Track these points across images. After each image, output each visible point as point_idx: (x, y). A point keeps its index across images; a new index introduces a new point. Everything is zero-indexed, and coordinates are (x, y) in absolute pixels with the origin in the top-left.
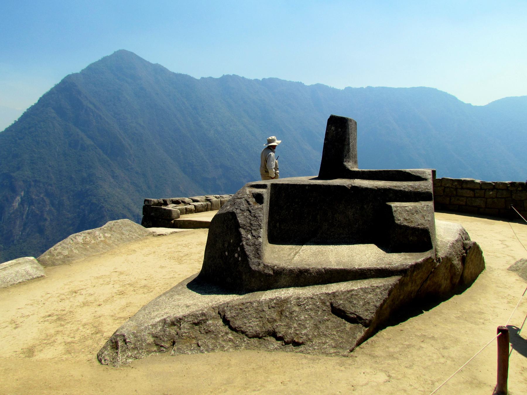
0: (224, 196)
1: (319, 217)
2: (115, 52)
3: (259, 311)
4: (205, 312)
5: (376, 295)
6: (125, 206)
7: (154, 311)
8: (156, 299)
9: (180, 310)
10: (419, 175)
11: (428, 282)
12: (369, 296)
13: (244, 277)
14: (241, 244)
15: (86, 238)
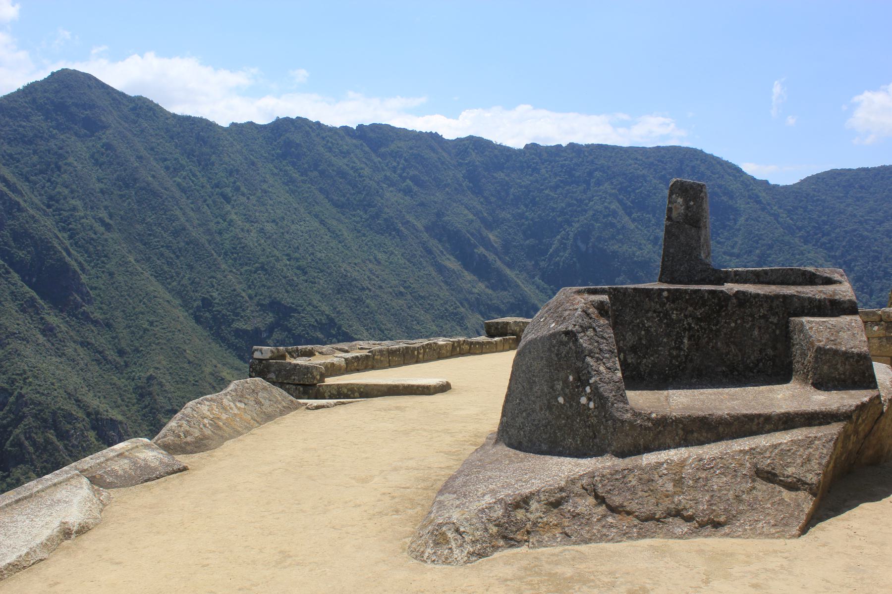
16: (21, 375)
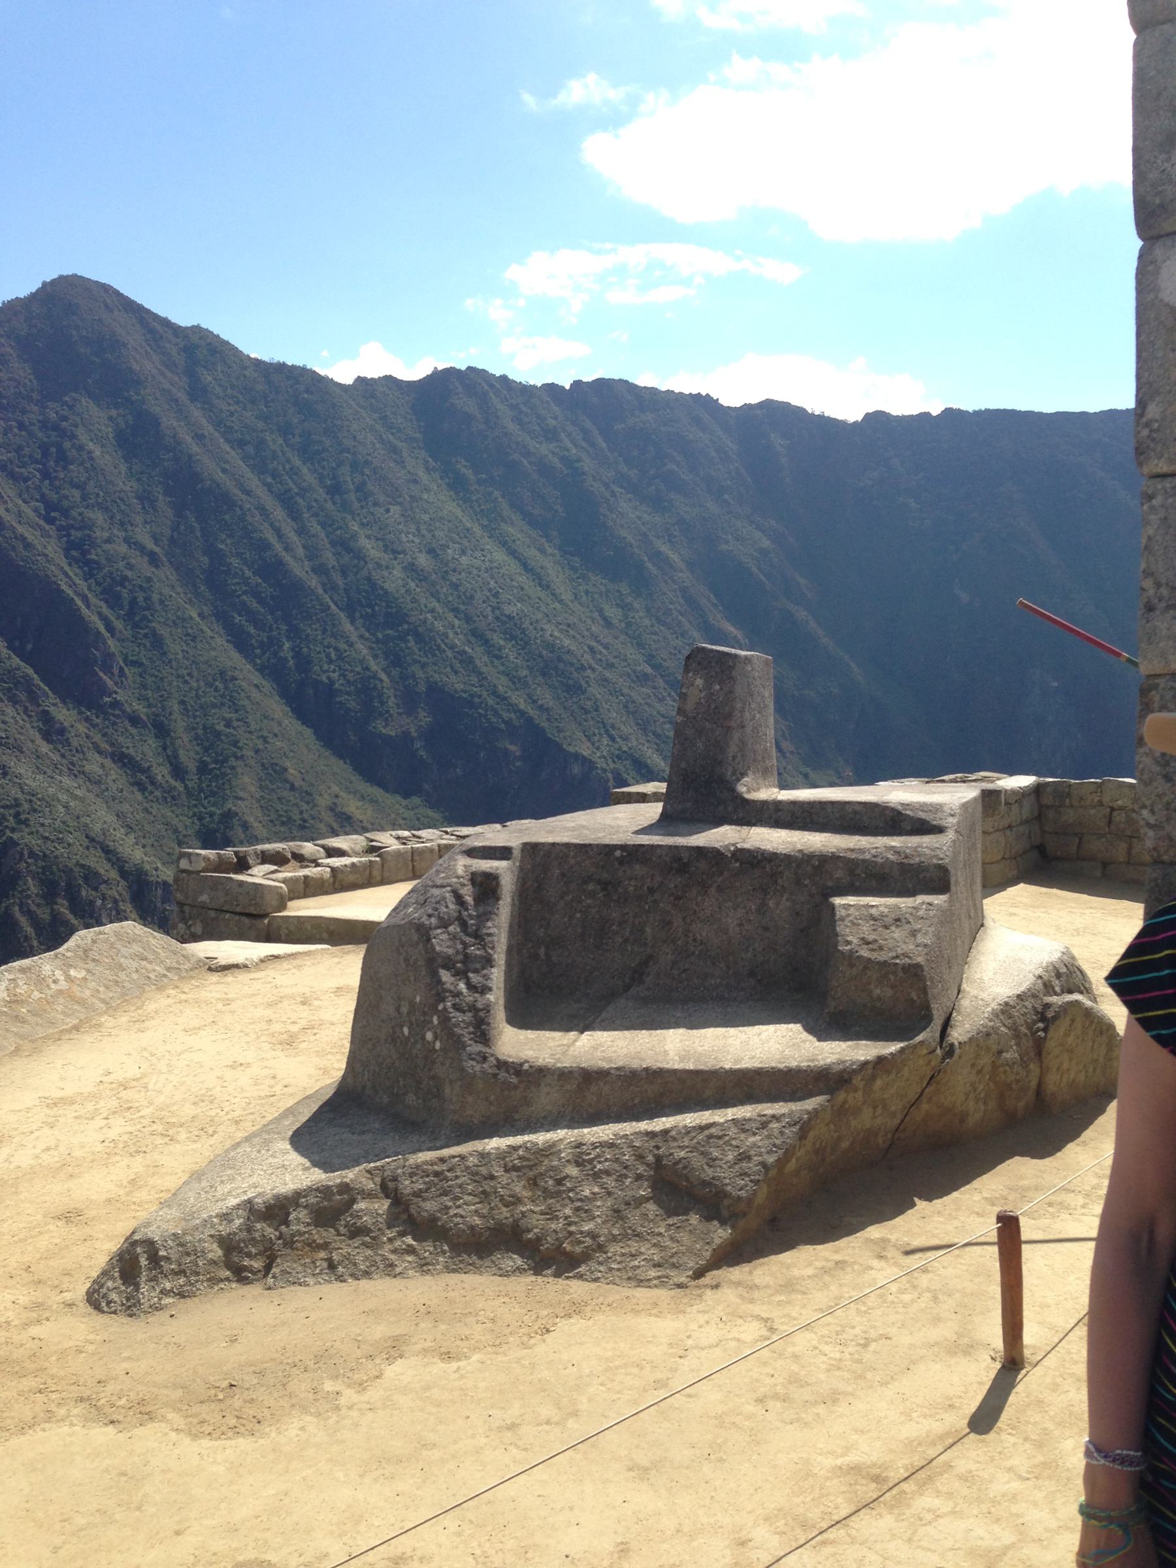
0: (424, 833)
1: (648, 930)
2: (45, 284)
3: (481, 1176)
4: (348, 1180)
5: (768, 1137)
6: (92, 840)
7: (222, 1182)
8: (227, 1151)
9: (288, 1178)
10: (922, 815)
11: (925, 1106)
12: (752, 1139)
13: (447, 1091)
14: (440, 1007)
15: (17, 986)
16: (11, 807)
